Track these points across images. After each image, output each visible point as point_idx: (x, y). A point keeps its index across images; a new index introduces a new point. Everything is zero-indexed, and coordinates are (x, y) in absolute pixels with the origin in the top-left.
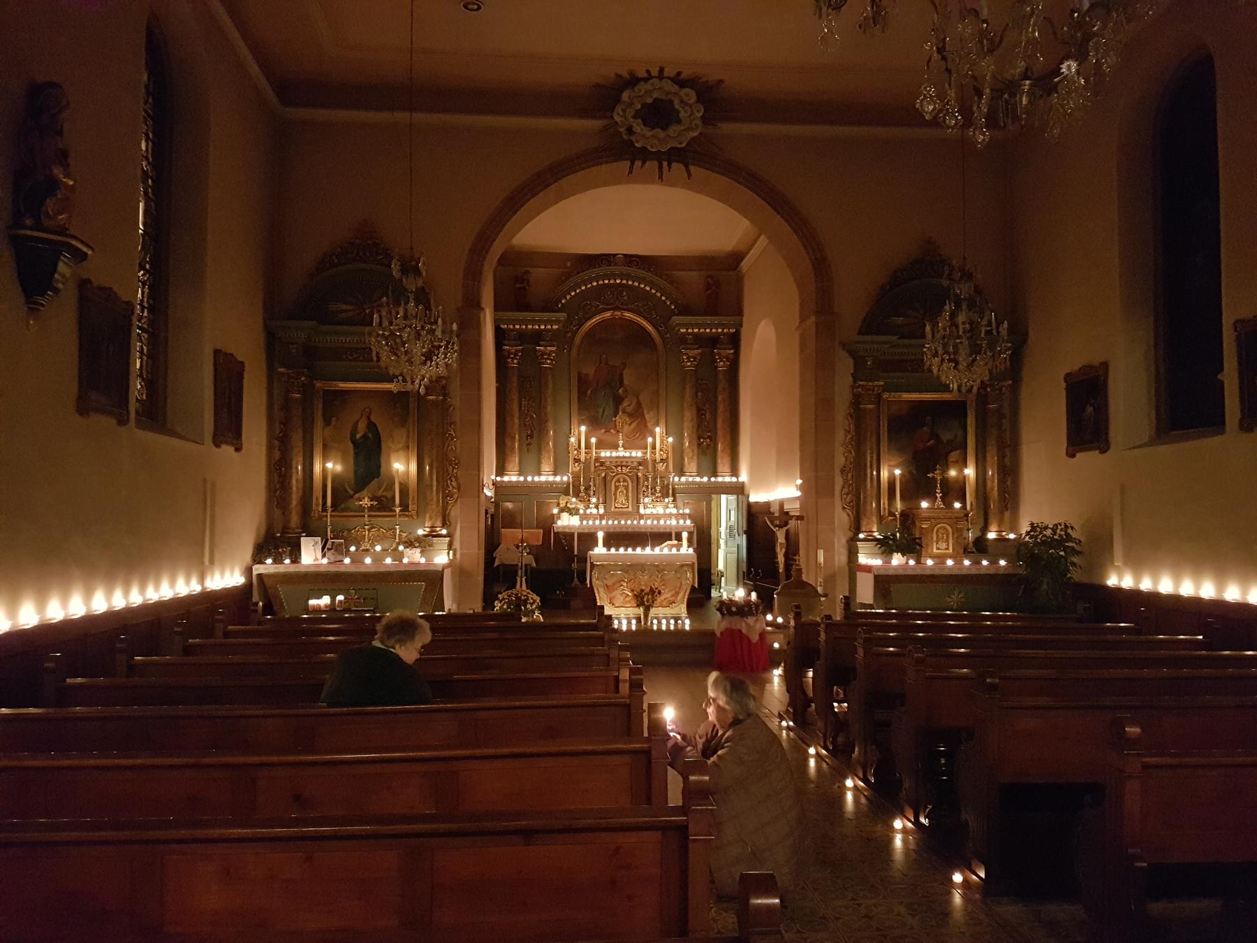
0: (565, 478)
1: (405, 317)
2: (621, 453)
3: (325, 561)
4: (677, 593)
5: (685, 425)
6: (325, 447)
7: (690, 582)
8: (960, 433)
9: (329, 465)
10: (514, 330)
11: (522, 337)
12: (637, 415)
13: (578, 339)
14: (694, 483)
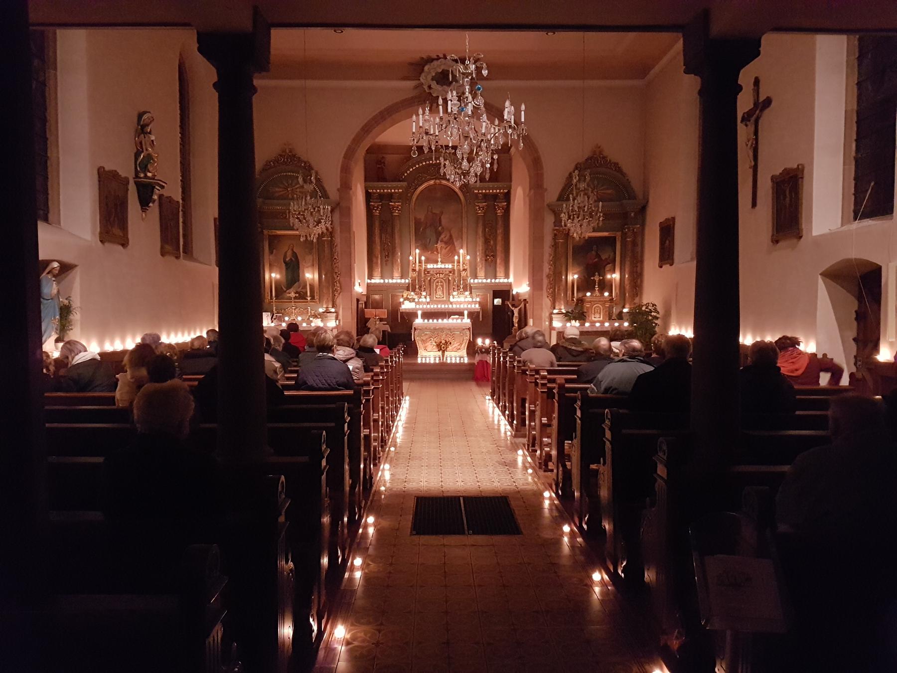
0: (407, 281)
1: (306, 204)
2: (440, 265)
3: (273, 325)
4: (461, 344)
6: (270, 265)
7: (468, 338)
8: (612, 254)
9: (273, 275)
10: (376, 193)
11: (381, 197)
12: (450, 242)
13: (415, 197)
14: (482, 283)
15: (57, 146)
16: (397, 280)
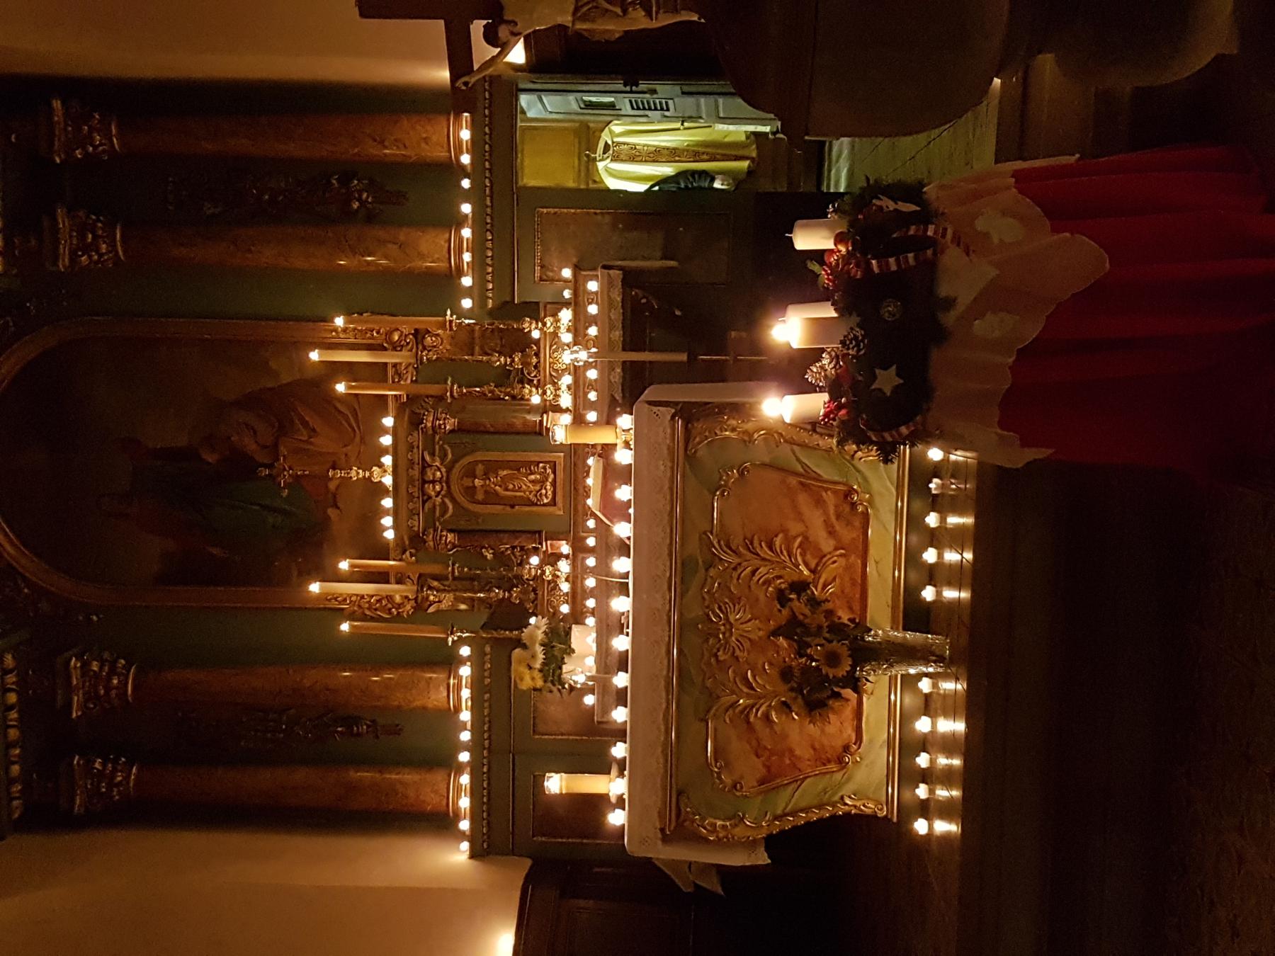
5: (300, 263)
14: (477, 247)
15: (894, 608)
16: (460, 691)
